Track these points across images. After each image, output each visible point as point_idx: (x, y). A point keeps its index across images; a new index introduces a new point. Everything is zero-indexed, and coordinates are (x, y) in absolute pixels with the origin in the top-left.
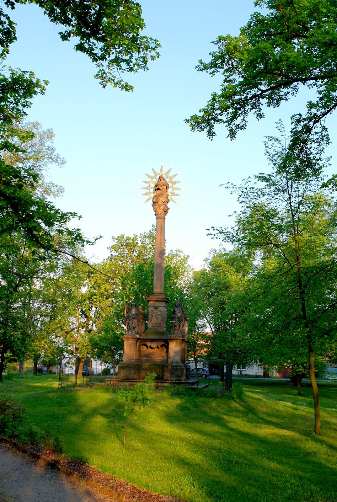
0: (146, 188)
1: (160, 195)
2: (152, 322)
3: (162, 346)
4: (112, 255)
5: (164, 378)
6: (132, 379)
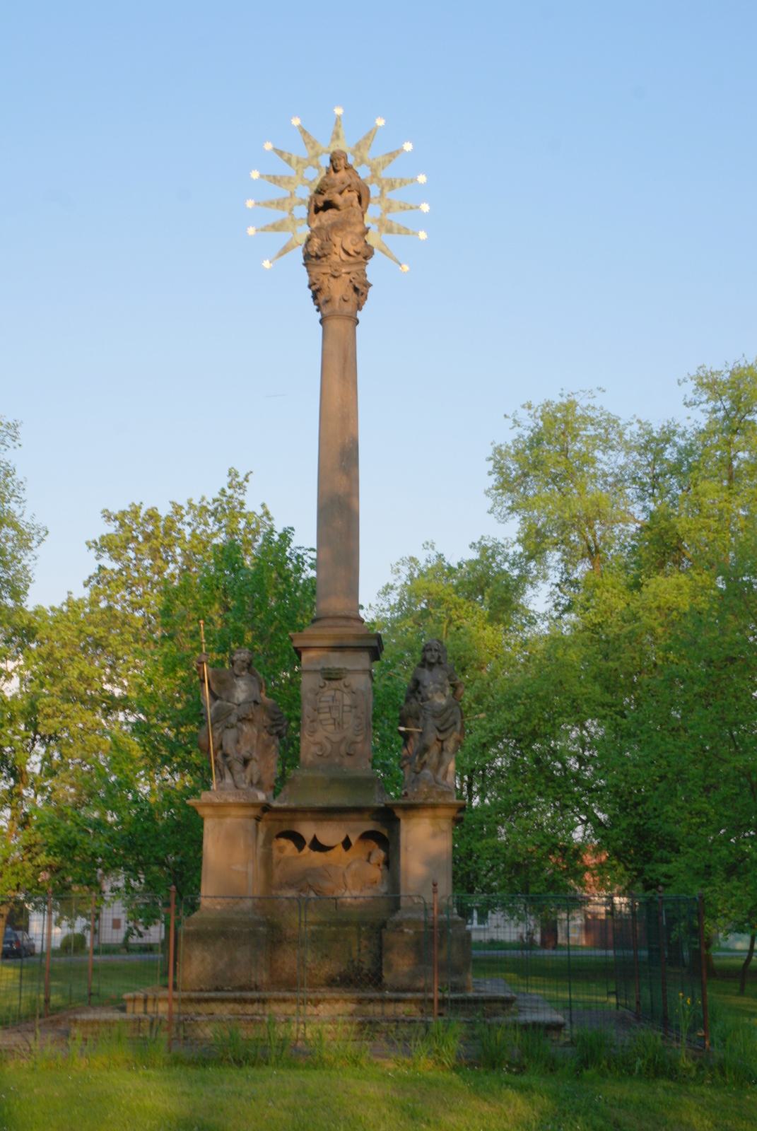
0: (279, 204)
1: (337, 226)
2: (319, 736)
3: (366, 836)
5: (387, 977)
6: (242, 988)
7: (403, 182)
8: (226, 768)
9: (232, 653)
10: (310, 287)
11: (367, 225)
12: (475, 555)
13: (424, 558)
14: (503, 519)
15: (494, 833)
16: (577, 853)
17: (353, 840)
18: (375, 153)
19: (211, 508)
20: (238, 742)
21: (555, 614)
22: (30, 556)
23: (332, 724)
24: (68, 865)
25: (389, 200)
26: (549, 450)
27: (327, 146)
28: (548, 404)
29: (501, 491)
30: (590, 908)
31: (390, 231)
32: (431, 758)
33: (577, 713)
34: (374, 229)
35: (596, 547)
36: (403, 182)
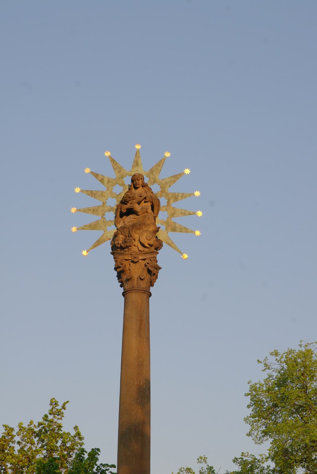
0: (94, 211)
7: (183, 196)
10: (116, 269)
11: (158, 225)
14: (259, 441)
18: (164, 175)
19: (36, 430)
25: (173, 208)
26: (293, 388)
27: (129, 170)
28: (290, 352)
29: (257, 418)
31: (174, 230)
34: (163, 228)
36: (183, 196)
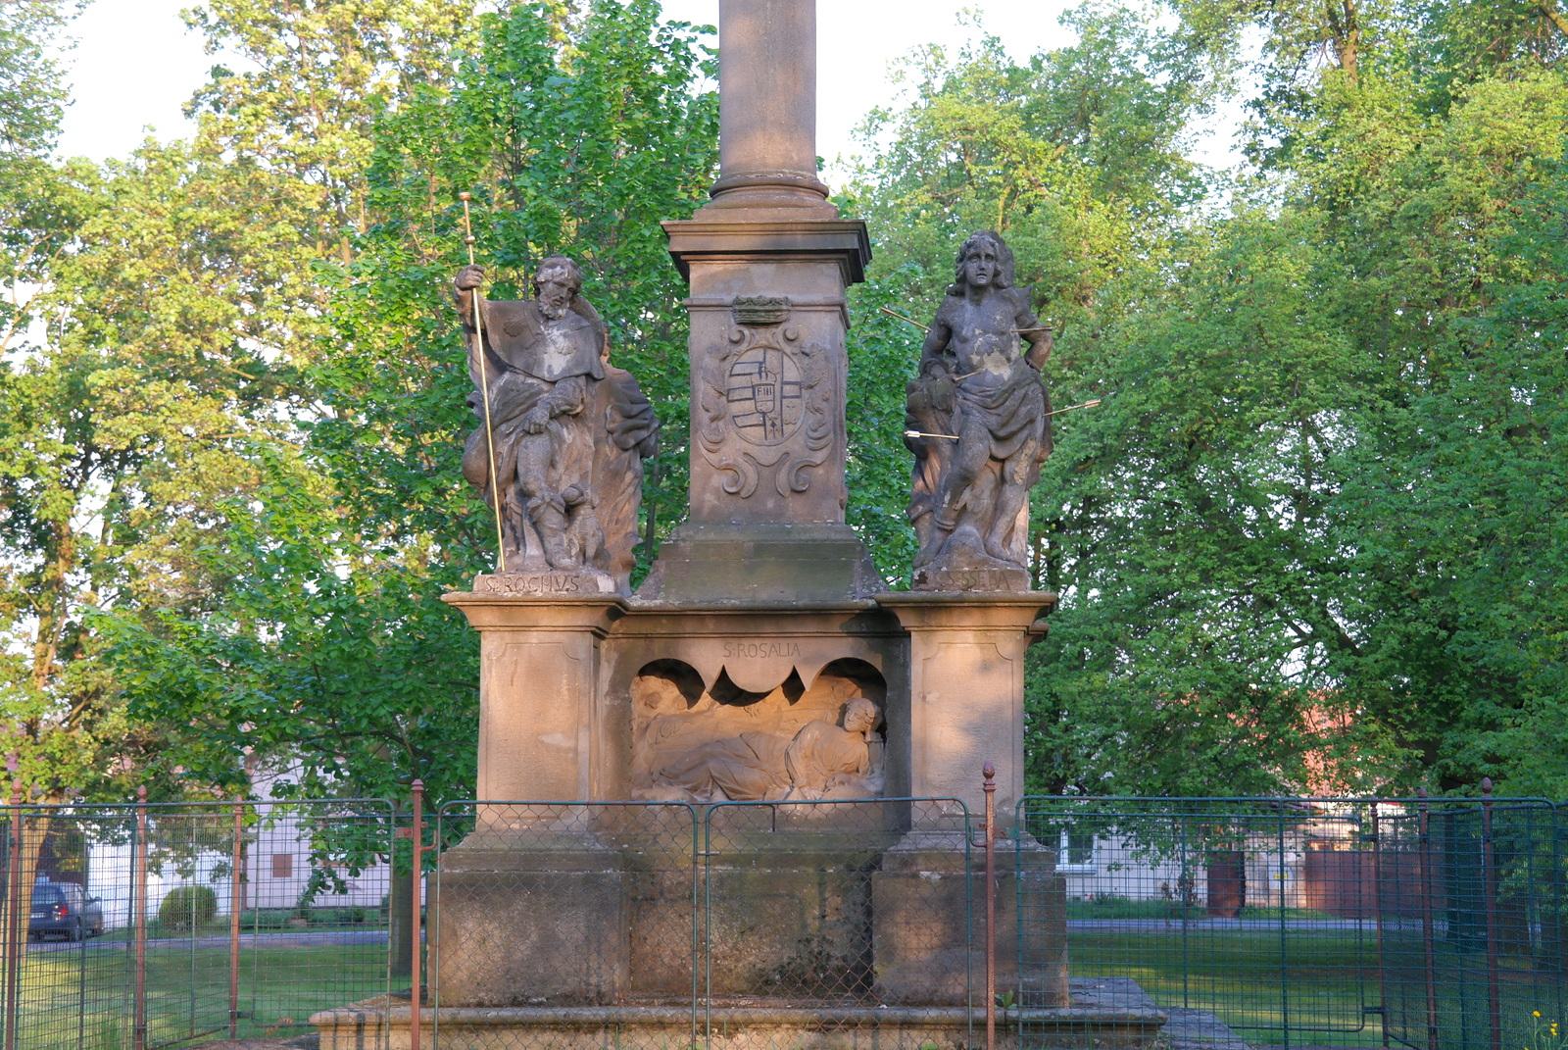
2: (730, 452)
3: (837, 670)
4: (217, 72)
5: (883, 973)
6: (568, 999)
8: (527, 523)
9: (534, 266)
12: (1071, 39)
13: (960, 46)
15: (1106, 662)
16: (1291, 708)
17: (808, 678)
20: (552, 464)
21: (1252, 170)
22: (60, 41)
23: (757, 429)
24: (173, 736)
30: (1320, 828)
32: (977, 498)
33: (1291, 394)
35: (1349, 13)
